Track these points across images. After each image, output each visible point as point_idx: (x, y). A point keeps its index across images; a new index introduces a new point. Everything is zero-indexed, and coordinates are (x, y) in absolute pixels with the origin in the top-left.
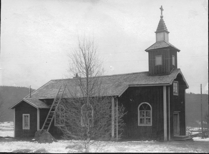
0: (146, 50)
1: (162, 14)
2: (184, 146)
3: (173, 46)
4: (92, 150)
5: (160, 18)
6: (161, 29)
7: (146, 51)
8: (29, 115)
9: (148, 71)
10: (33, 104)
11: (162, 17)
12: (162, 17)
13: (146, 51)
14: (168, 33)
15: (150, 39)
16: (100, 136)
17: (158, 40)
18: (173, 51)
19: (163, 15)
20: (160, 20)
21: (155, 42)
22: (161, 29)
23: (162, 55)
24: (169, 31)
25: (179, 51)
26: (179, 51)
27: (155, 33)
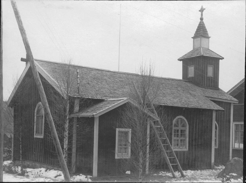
0: (178, 60)
1: (202, 15)
2: (59, 148)
3: (28, 41)
4: (166, 182)
5: (200, 21)
6: (201, 32)
7: (180, 60)
9: (25, 62)
10: (104, 109)
11: (202, 19)
12: (202, 19)
13: (180, 60)
14: (209, 38)
15: (187, 47)
16: (45, 125)
17: (195, 47)
18: (215, 61)
19: (204, 17)
20: (200, 22)
21: (192, 49)
22: (201, 32)
23: (194, 66)
25: (223, 58)
26: (223, 58)
27: (192, 39)
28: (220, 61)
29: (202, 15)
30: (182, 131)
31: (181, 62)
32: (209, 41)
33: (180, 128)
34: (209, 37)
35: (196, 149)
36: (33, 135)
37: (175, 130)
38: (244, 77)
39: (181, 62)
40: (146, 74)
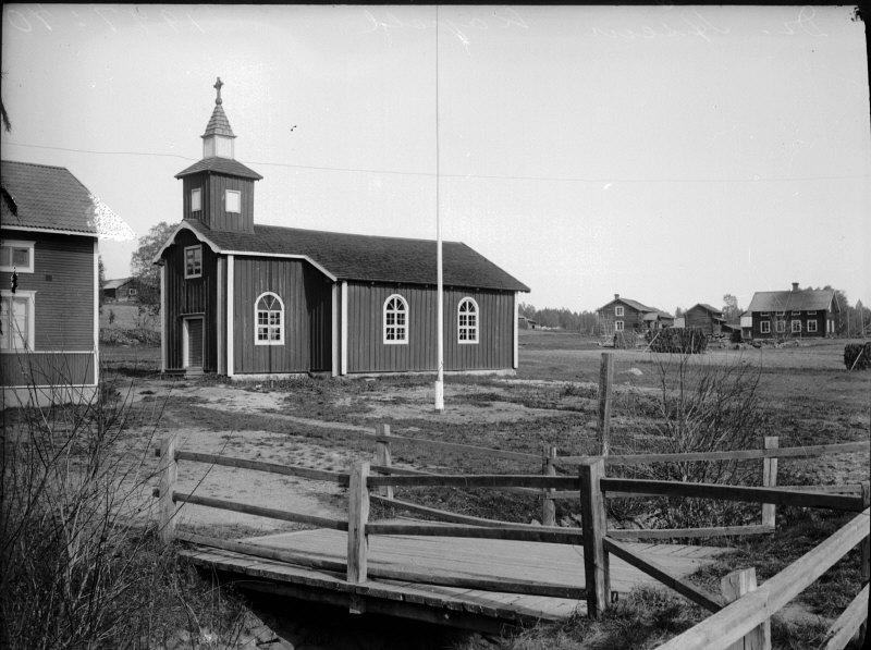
1: (219, 94)
6: (217, 127)
7: (178, 177)
8: (477, 341)
11: (219, 102)
12: (219, 102)
15: (193, 154)
18: (244, 179)
22: (217, 127)
24: (235, 133)
26: (259, 178)
28: (256, 182)
29: (219, 94)
30: (470, 317)
31: (181, 181)
32: (233, 146)
33: (467, 313)
34: (234, 137)
35: (145, 395)
36: (253, 341)
37: (461, 317)
38: (868, 532)
39: (181, 181)
40: (378, 289)
